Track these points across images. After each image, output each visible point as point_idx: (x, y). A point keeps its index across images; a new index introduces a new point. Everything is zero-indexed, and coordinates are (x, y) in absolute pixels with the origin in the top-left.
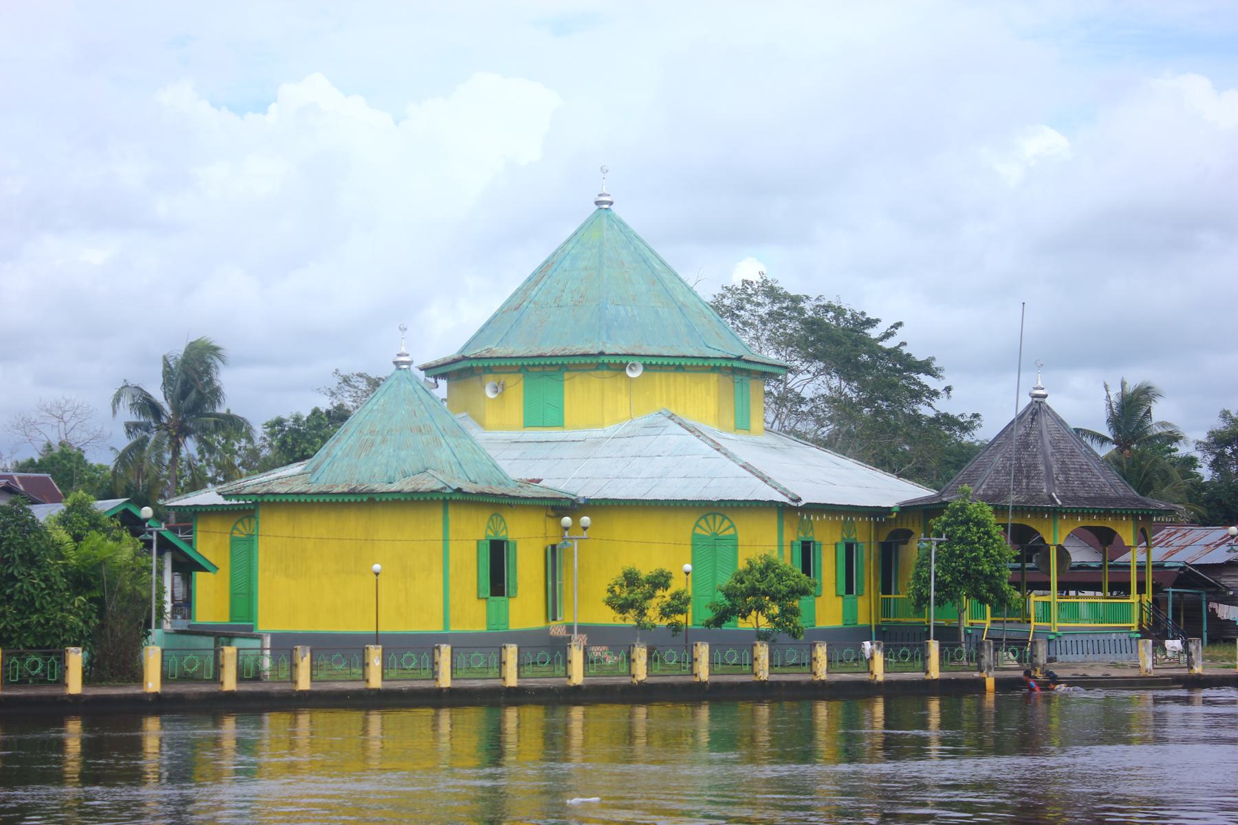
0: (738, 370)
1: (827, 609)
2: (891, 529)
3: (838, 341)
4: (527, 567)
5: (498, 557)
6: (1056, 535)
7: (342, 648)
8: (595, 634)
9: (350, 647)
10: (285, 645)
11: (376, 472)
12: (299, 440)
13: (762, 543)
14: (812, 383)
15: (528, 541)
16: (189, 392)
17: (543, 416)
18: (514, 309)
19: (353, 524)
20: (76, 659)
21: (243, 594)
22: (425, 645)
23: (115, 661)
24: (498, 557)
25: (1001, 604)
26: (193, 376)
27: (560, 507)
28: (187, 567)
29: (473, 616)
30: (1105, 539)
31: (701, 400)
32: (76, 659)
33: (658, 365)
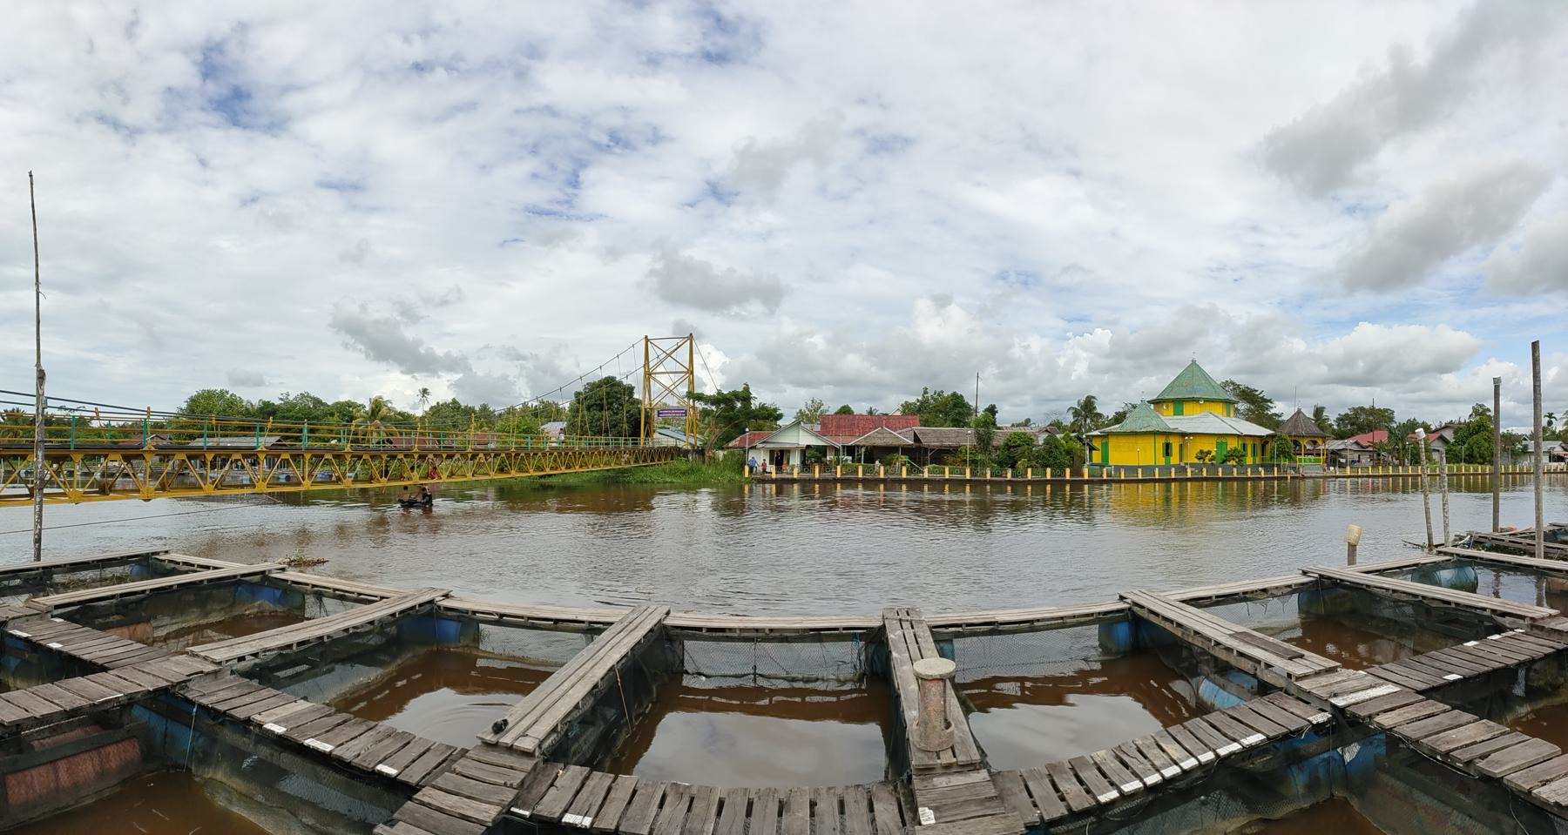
0: (1227, 402)
1: (1249, 460)
2: (1264, 441)
3: (1248, 395)
4: (1175, 449)
5: (1167, 446)
6: (1304, 442)
7: (1131, 469)
8: (1192, 465)
9: (1134, 469)
10: (1118, 468)
11: (1137, 427)
12: (1120, 417)
13: (1233, 444)
14: (1243, 406)
15: (1175, 444)
16: (1087, 407)
17: (1179, 412)
18: (1170, 387)
19: (1132, 439)
20: (1068, 471)
21: (1105, 457)
22: (1152, 468)
23: (1077, 472)
24: (1167, 446)
25: (1291, 459)
26: (1088, 406)
27: (1183, 435)
28: (1092, 449)
29: (1161, 461)
30: (1315, 443)
31: (1219, 409)
32: (1068, 471)
33: (1207, 401)
